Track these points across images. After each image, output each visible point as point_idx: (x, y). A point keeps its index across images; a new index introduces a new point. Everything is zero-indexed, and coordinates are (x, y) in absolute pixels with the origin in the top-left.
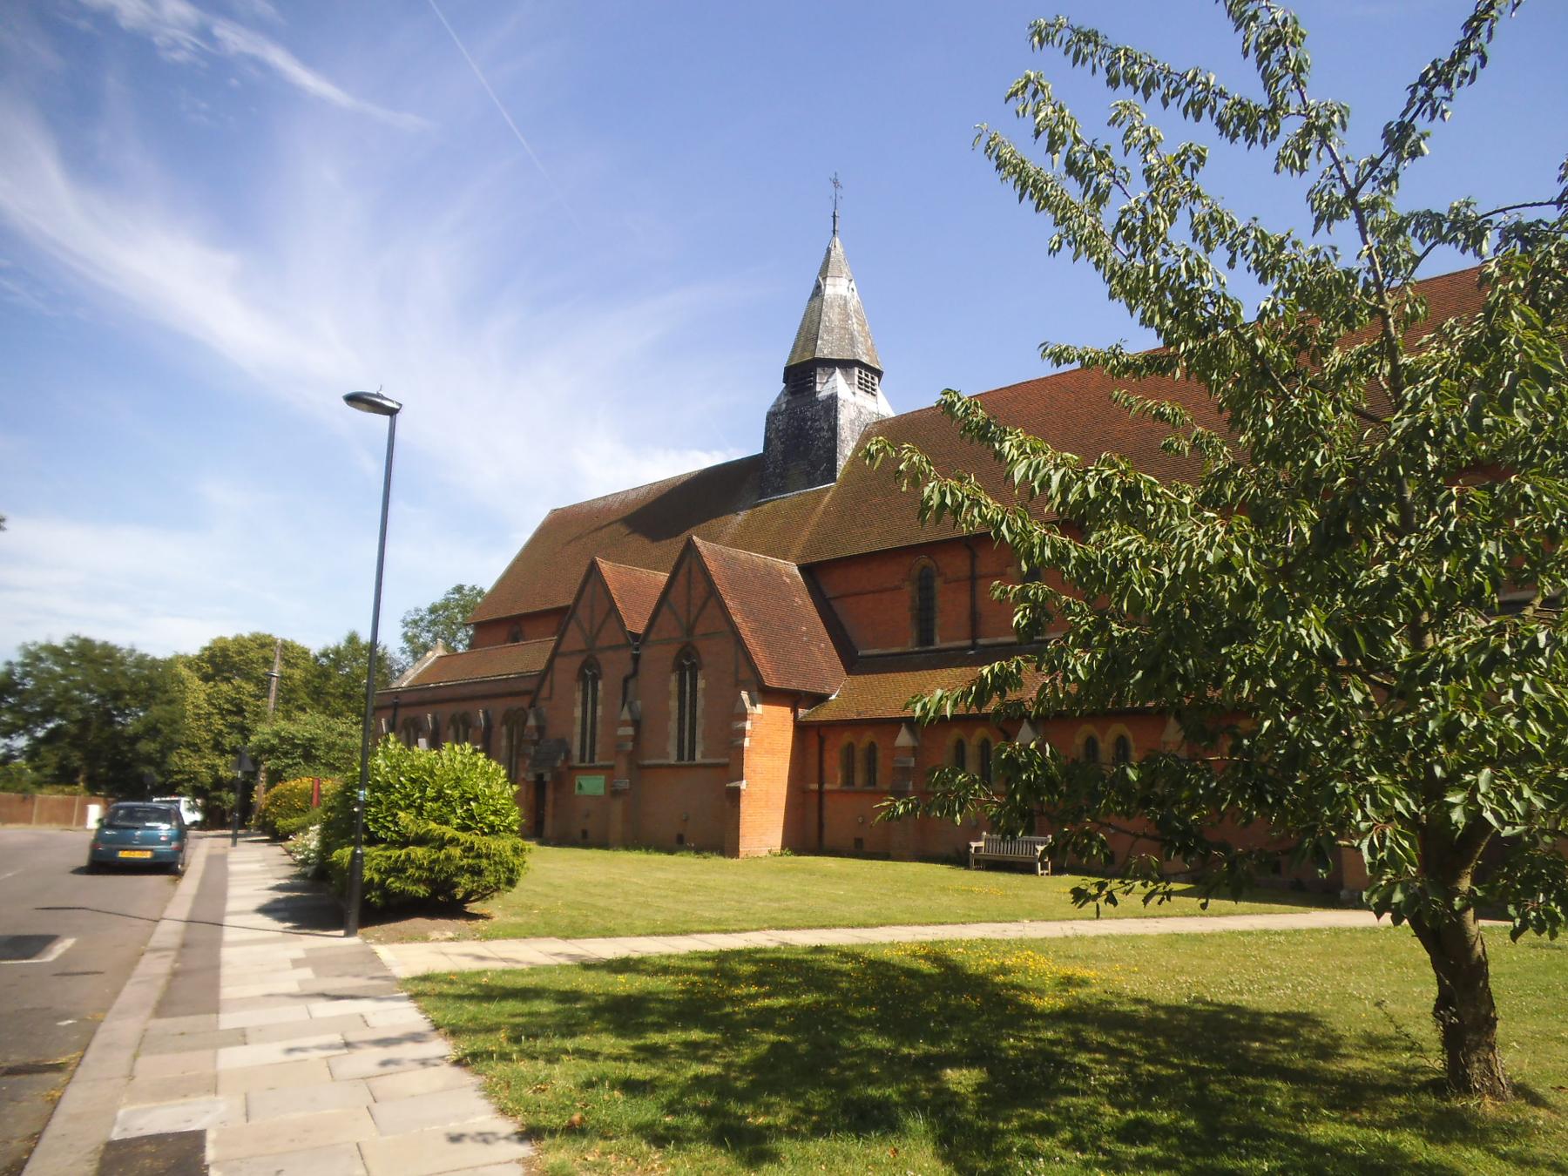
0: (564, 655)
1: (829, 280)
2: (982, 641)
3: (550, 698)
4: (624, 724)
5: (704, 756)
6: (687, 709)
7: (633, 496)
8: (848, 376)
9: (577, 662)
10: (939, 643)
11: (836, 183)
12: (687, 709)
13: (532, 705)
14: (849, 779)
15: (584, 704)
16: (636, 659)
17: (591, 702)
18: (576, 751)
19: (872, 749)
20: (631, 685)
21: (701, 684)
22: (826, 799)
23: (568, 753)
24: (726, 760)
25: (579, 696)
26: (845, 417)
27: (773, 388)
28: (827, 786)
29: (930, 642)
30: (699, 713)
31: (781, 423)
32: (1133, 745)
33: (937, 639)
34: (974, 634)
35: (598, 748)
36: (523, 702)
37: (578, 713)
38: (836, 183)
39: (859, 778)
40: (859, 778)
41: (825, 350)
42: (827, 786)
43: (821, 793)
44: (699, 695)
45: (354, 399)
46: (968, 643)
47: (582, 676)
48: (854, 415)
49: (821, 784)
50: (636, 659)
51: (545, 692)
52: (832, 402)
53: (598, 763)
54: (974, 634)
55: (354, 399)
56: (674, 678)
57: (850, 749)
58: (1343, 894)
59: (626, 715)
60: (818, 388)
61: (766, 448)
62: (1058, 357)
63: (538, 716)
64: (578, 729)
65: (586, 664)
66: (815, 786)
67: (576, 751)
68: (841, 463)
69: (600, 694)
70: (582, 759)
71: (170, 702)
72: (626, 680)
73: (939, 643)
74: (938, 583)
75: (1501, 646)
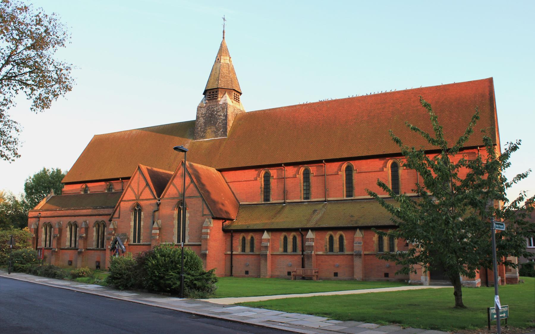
0: (125, 201)
1: (222, 57)
2: (288, 201)
3: (119, 218)
4: (156, 229)
5: (189, 242)
7: (134, 132)
8: (230, 94)
10: (272, 201)
11: (224, 19)
12: (48, 236)
14: (243, 250)
15: (135, 221)
21: (187, 215)
22: (234, 257)
23: (128, 239)
24: (199, 243)
25: (133, 218)
26: (230, 111)
27: (198, 97)
28: (234, 253)
29: (269, 200)
30: (187, 226)
31: (203, 111)
32: (345, 238)
33: (271, 200)
35: (142, 238)
37: (132, 223)
38: (224, 19)
39: (248, 249)
40: (248, 249)
41: (222, 85)
42: (234, 253)
44: (187, 219)
45: (176, 149)
46: (283, 201)
48: (232, 110)
49: (232, 252)
51: (116, 215)
52: (225, 106)
53: (141, 243)
55: (176, 149)
57: (244, 239)
58: (409, 282)
60: (219, 99)
61: (198, 117)
64: (132, 230)
66: (229, 253)
67: (132, 238)
68: (229, 129)
69: (142, 217)
70: (134, 241)
73: (272, 201)
75: (152, 263)
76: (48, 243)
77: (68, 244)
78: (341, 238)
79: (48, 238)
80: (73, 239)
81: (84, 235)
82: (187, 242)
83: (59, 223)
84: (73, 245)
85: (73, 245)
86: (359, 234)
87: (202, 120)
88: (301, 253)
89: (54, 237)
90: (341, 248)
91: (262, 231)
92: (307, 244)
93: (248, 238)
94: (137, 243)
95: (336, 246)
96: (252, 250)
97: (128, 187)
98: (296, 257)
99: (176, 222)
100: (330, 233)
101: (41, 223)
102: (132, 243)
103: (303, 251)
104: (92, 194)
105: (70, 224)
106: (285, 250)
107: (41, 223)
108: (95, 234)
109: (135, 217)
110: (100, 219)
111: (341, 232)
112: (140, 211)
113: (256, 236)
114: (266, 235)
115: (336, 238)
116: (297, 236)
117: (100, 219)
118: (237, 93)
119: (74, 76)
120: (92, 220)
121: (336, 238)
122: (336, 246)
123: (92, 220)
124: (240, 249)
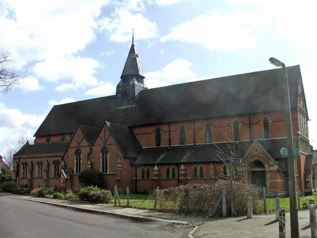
2: (171, 146)
4: (89, 164)
6: (40, 170)
9: (75, 149)
10: (162, 146)
12: (40, 170)
13: (62, 159)
16: (91, 149)
17: (79, 159)
18: (75, 170)
19: (148, 170)
20: (90, 155)
21: (108, 156)
25: (75, 158)
34: (170, 144)
36: (60, 159)
37: (75, 162)
39: (145, 177)
40: (145, 177)
43: (136, 180)
46: (193, 144)
47: (76, 153)
50: (91, 149)
51: (66, 156)
52: (134, 86)
54: (170, 144)
56: (101, 154)
59: (89, 162)
62: (273, 60)
63: (64, 162)
65: (77, 150)
67: (75, 170)
70: (77, 173)
71: (127, 4)
72: (89, 154)
74: (162, 132)
76: (25, 174)
77: (37, 175)
78: (201, 168)
79: (25, 172)
80: (25, 172)
81: (47, 169)
82: (108, 173)
83: (32, 162)
84: (40, 176)
85: (40, 176)
86: (212, 166)
87: (120, 95)
88: (177, 178)
89: (45, 171)
90: (202, 175)
91: (154, 165)
92: (181, 172)
93: (146, 169)
94: (105, 173)
95: (198, 173)
96: (148, 177)
97: (98, 136)
98: (174, 181)
99: (101, 160)
100: (168, 166)
101: (21, 162)
102: (75, 173)
103: (179, 177)
104: (53, 144)
105: (55, 163)
106: (168, 176)
107: (21, 162)
108: (53, 168)
109: (77, 157)
110: (56, 159)
111: (148, 167)
112: (106, 152)
113: (150, 169)
114: (156, 168)
115: (198, 169)
116: (175, 168)
117: (56, 159)
118: (141, 79)
119: (268, 61)
120: (51, 160)
121: (198, 169)
122: (198, 173)
123: (51, 160)
124: (165, 176)
